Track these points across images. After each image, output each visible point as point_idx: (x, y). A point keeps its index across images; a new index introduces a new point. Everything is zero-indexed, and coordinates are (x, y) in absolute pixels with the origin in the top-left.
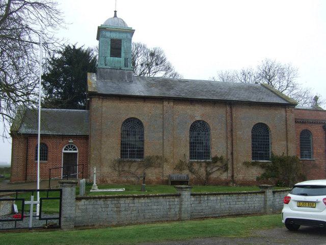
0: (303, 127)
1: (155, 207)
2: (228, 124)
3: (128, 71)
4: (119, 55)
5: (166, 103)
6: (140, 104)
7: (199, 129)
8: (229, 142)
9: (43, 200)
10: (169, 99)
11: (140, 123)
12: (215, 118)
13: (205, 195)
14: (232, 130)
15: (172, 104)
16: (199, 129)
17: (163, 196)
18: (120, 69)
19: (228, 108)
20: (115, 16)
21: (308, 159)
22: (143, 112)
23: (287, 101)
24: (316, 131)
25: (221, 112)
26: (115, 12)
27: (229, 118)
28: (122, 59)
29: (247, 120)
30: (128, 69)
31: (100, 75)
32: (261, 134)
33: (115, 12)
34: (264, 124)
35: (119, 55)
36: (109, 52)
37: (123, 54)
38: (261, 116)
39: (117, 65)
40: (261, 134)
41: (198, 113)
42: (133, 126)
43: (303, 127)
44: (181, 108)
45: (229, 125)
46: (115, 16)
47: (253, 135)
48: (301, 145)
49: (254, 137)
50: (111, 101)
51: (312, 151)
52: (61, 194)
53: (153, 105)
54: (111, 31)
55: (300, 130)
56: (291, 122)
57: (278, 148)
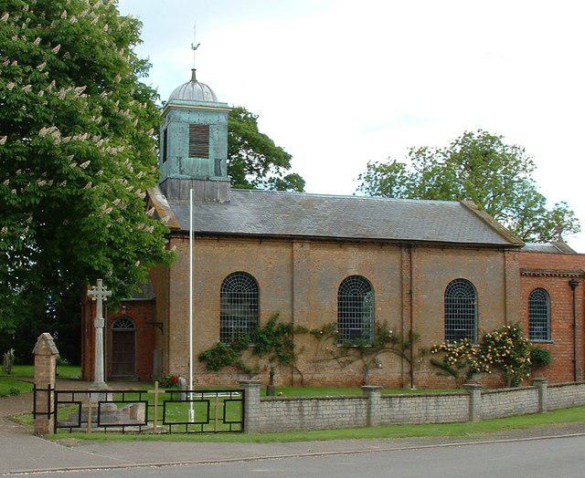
0: (534, 283)
1: (339, 411)
2: (404, 282)
3: (223, 184)
4: (204, 154)
5: (297, 246)
6: (253, 248)
7: (354, 291)
8: (406, 313)
9: (58, 405)
10: (302, 239)
11: (252, 283)
12: (380, 269)
13: (397, 397)
14: (411, 293)
15: (307, 247)
16: (354, 291)
17: (557, 386)
18: (208, 180)
19: (405, 255)
20: (194, 80)
21: (542, 341)
22: (259, 262)
23: (506, 239)
24: (557, 288)
25: (391, 259)
26: (194, 70)
27: (406, 272)
28: (210, 161)
29: (435, 275)
30: (221, 179)
31: (172, 190)
32: (460, 299)
33: (194, 70)
34: (467, 281)
35: (204, 154)
36: (187, 148)
37: (211, 153)
38: (462, 267)
39: (202, 173)
40: (460, 299)
41: (355, 262)
42: (241, 289)
43: (534, 283)
44: (322, 253)
45: (406, 283)
46: (194, 80)
47: (446, 301)
48: (530, 316)
49: (449, 304)
50: (203, 243)
51: (549, 325)
52: (243, 395)
53: (274, 249)
54: (190, 111)
55: (529, 289)
56: (513, 275)
57: (488, 322)
